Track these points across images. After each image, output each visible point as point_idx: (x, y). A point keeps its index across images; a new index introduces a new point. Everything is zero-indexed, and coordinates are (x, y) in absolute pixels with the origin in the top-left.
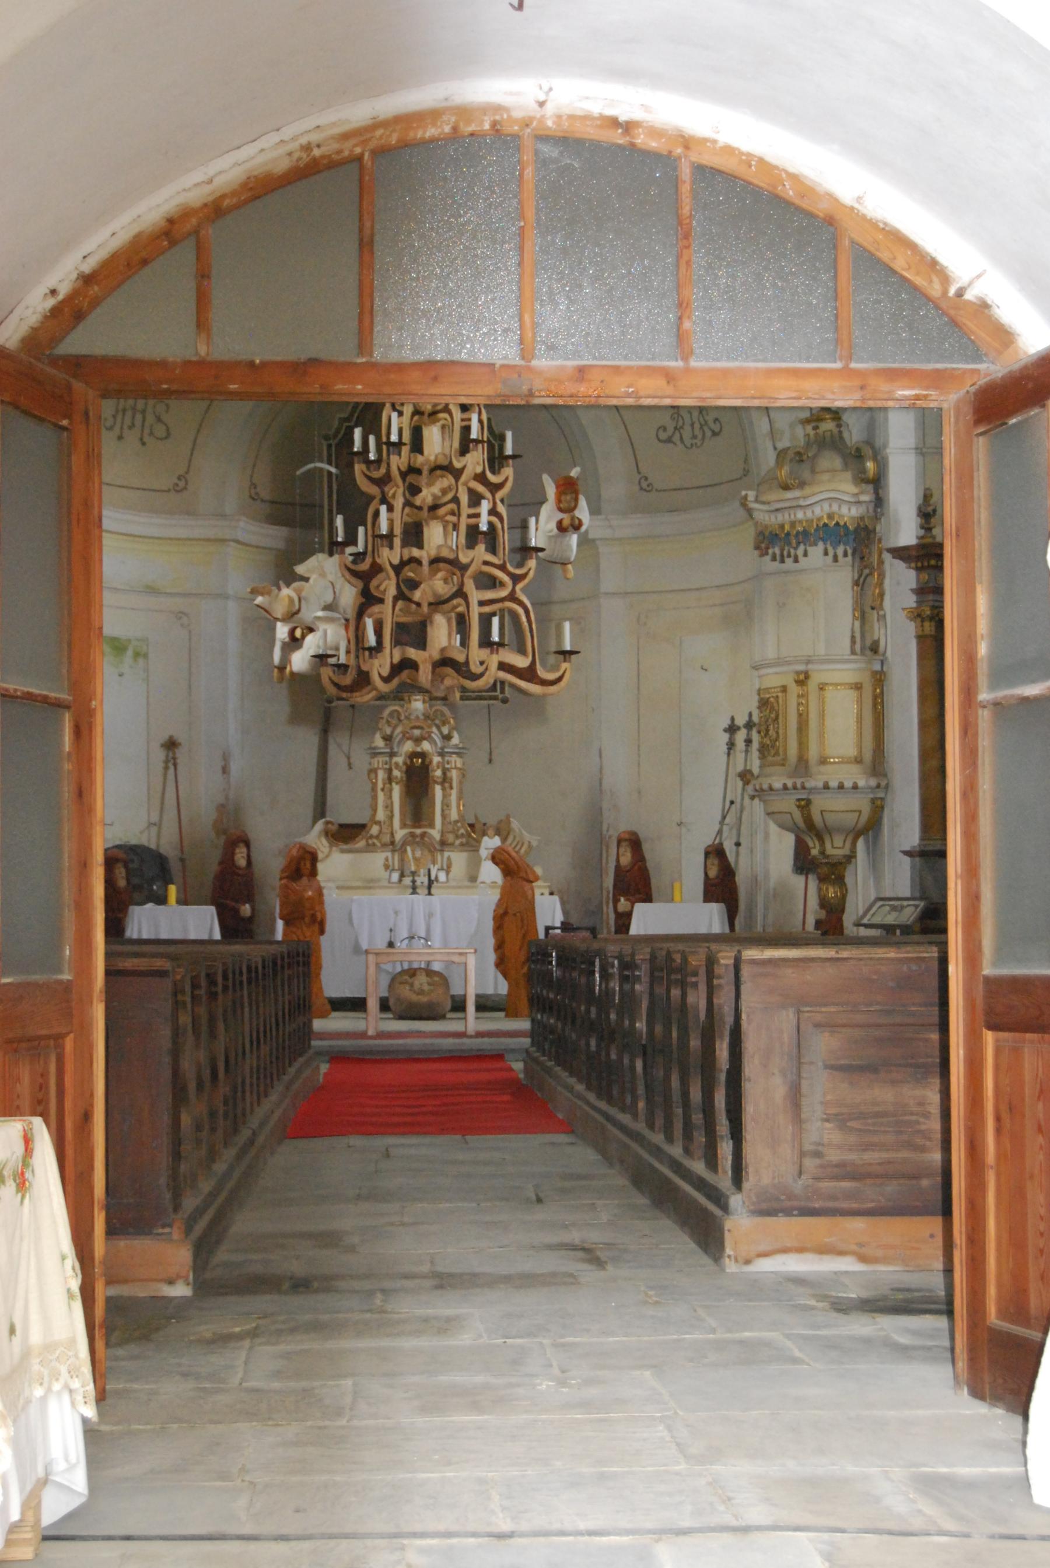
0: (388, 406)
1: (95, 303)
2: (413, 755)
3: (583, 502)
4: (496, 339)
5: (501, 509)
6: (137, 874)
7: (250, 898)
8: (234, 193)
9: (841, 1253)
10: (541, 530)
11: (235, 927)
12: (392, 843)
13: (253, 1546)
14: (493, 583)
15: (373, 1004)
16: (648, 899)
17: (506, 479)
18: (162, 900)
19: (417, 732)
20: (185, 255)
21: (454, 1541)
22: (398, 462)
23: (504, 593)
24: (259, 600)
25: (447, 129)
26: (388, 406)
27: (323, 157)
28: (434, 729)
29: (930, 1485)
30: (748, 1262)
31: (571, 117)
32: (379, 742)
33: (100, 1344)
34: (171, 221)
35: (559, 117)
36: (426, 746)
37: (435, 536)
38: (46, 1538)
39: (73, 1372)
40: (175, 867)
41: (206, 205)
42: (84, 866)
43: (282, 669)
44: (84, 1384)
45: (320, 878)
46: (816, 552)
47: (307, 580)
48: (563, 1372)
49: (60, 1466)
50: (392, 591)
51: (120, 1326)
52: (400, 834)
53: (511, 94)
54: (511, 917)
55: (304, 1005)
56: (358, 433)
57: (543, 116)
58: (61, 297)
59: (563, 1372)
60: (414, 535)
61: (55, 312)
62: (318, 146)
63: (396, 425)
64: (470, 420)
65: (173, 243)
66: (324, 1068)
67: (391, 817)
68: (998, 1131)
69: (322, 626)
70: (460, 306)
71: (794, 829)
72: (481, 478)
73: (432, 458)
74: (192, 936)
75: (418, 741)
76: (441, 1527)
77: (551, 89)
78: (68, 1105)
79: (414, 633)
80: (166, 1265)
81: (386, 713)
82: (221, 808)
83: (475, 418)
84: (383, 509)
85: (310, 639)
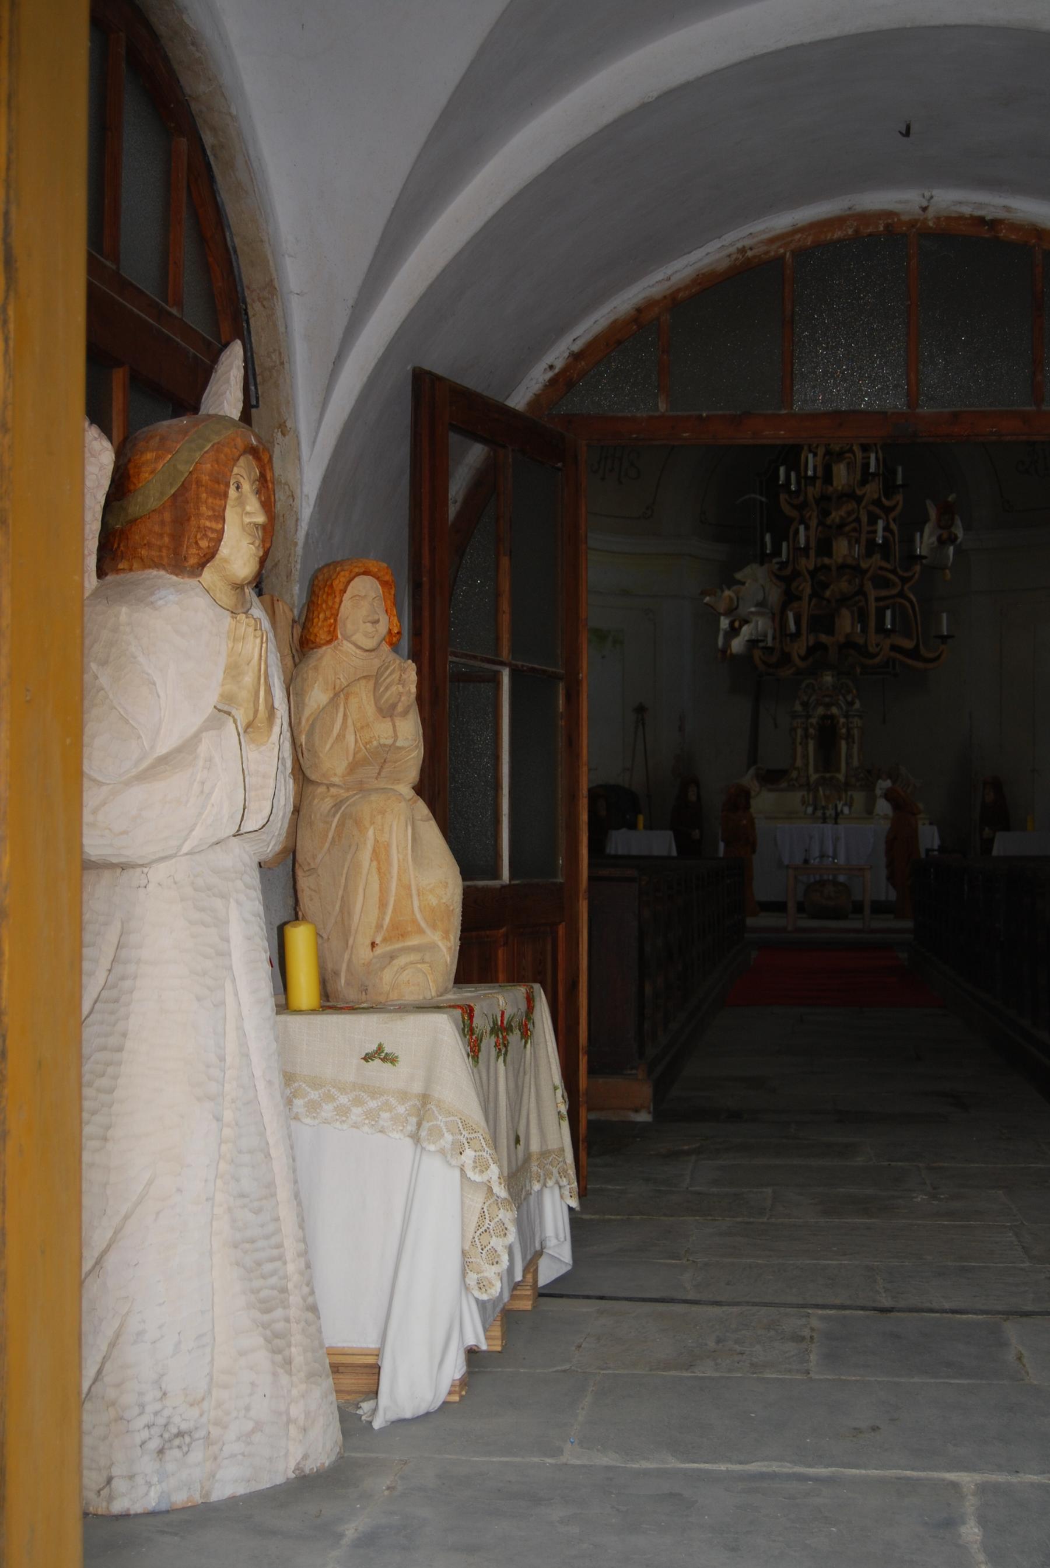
0: (806, 448)
2: (824, 717)
3: (958, 522)
4: (888, 393)
5: (894, 527)
6: (613, 807)
8: (687, 287)
10: (925, 542)
11: (687, 847)
12: (808, 784)
13: (694, 1308)
14: (887, 584)
15: (791, 906)
16: (1007, 828)
17: (898, 503)
18: (633, 826)
19: (827, 700)
21: (847, 1312)
22: (813, 492)
23: (895, 591)
24: (707, 599)
25: (850, 232)
26: (806, 448)
27: (754, 257)
28: (841, 697)
31: (948, 218)
32: (798, 708)
33: (583, 1155)
34: (639, 310)
35: (938, 218)
36: (834, 710)
37: (841, 548)
38: (541, 1295)
39: (563, 1173)
41: (665, 297)
42: (573, 797)
43: (724, 651)
44: (570, 1184)
45: (752, 810)
47: (743, 584)
48: (934, 1188)
49: (551, 1242)
50: (808, 591)
51: (598, 1143)
52: (814, 777)
53: (900, 202)
54: (900, 841)
56: (782, 470)
57: (926, 219)
58: (557, 370)
59: (934, 1188)
60: (825, 547)
61: (553, 382)
62: (751, 249)
63: (811, 464)
64: (869, 458)
67: (807, 765)
69: (754, 619)
70: (860, 368)
72: (877, 502)
73: (840, 488)
74: (656, 853)
75: (828, 706)
76: (838, 1302)
77: (932, 197)
78: (561, 976)
79: (823, 623)
80: (634, 1102)
81: (804, 685)
83: (873, 456)
84: (802, 528)
85: (745, 629)
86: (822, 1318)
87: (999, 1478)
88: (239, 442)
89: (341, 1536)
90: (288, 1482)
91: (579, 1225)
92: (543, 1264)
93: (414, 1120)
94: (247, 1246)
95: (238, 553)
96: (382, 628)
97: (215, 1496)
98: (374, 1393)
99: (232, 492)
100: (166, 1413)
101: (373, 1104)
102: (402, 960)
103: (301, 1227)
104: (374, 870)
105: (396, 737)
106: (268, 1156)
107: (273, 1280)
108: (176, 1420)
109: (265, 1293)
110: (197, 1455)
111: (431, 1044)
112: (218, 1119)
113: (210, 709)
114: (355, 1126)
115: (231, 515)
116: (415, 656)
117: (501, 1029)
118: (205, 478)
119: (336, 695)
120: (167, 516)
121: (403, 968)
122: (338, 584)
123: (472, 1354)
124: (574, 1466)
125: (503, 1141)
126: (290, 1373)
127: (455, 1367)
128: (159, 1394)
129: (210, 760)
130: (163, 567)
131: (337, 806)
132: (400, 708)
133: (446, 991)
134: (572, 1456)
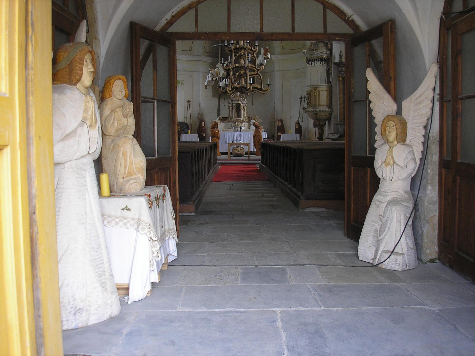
1: (175, 21)
7: (205, 133)
9: (322, 207)
11: (202, 139)
13: (209, 267)
14: (252, 71)
15: (229, 153)
16: (284, 133)
18: (187, 133)
20: (192, 12)
29: (339, 256)
30: (304, 209)
33: (178, 227)
36: (240, 102)
40: (190, 126)
46: (318, 63)
51: (181, 222)
54: (257, 137)
55: (215, 155)
61: (167, 23)
65: (190, 9)
66: (220, 167)
68: (354, 186)
71: (313, 119)
75: (238, 100)
76: (245, 264)
82: (199, 114)
86: (241, 269)
87: (286, 309)
88: (86, 50)
89: (122, 333)
90: (108, 319)
91: (179, 246)
92: (169, 257)
93: (136, 225)
94: (94, 261)
95: (87, 79)
96: (124, 93)
97: (89, 324)
98: (128, 294)
99: (85, 63)
100: (76, 304)
101: (125, 221)
102: (131, 182)
103: (108, 255)
104: (123, 159)
105: (128, 122)
106: (99, 237)
107: (101, 269)
108: (78, 306)
109: (99, 273)
110: (84, 314)
111: (139, 205)
112: (85, 229)
113: (80, 121)
114: (120, 227)
115: (85, 69)
116: (132, 101)
117: (157, 199)
118: (78, 60)
119: (112, 112)
120: (67, 70)
121: (131, 184)
122: (112, 82)
123: (153, 284)
124: (180, 312)
125: (159, 228)
126: (107, 292)
127: (149, 288)
128: (73, 300)
129: (80, 135)
130: (67, 83)
131: (113, 141)
132: (129, 115)
133: (142, 189)
134: (180, 309)
